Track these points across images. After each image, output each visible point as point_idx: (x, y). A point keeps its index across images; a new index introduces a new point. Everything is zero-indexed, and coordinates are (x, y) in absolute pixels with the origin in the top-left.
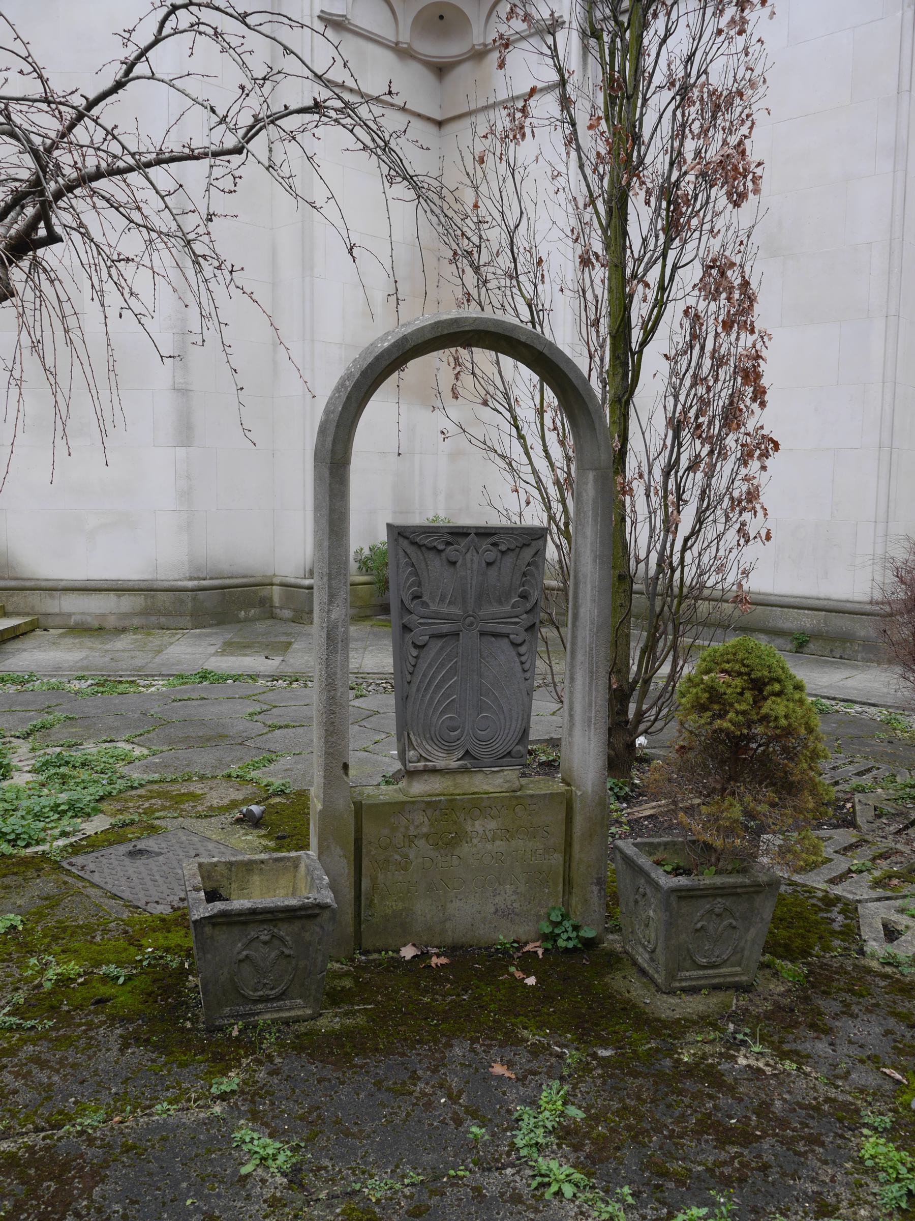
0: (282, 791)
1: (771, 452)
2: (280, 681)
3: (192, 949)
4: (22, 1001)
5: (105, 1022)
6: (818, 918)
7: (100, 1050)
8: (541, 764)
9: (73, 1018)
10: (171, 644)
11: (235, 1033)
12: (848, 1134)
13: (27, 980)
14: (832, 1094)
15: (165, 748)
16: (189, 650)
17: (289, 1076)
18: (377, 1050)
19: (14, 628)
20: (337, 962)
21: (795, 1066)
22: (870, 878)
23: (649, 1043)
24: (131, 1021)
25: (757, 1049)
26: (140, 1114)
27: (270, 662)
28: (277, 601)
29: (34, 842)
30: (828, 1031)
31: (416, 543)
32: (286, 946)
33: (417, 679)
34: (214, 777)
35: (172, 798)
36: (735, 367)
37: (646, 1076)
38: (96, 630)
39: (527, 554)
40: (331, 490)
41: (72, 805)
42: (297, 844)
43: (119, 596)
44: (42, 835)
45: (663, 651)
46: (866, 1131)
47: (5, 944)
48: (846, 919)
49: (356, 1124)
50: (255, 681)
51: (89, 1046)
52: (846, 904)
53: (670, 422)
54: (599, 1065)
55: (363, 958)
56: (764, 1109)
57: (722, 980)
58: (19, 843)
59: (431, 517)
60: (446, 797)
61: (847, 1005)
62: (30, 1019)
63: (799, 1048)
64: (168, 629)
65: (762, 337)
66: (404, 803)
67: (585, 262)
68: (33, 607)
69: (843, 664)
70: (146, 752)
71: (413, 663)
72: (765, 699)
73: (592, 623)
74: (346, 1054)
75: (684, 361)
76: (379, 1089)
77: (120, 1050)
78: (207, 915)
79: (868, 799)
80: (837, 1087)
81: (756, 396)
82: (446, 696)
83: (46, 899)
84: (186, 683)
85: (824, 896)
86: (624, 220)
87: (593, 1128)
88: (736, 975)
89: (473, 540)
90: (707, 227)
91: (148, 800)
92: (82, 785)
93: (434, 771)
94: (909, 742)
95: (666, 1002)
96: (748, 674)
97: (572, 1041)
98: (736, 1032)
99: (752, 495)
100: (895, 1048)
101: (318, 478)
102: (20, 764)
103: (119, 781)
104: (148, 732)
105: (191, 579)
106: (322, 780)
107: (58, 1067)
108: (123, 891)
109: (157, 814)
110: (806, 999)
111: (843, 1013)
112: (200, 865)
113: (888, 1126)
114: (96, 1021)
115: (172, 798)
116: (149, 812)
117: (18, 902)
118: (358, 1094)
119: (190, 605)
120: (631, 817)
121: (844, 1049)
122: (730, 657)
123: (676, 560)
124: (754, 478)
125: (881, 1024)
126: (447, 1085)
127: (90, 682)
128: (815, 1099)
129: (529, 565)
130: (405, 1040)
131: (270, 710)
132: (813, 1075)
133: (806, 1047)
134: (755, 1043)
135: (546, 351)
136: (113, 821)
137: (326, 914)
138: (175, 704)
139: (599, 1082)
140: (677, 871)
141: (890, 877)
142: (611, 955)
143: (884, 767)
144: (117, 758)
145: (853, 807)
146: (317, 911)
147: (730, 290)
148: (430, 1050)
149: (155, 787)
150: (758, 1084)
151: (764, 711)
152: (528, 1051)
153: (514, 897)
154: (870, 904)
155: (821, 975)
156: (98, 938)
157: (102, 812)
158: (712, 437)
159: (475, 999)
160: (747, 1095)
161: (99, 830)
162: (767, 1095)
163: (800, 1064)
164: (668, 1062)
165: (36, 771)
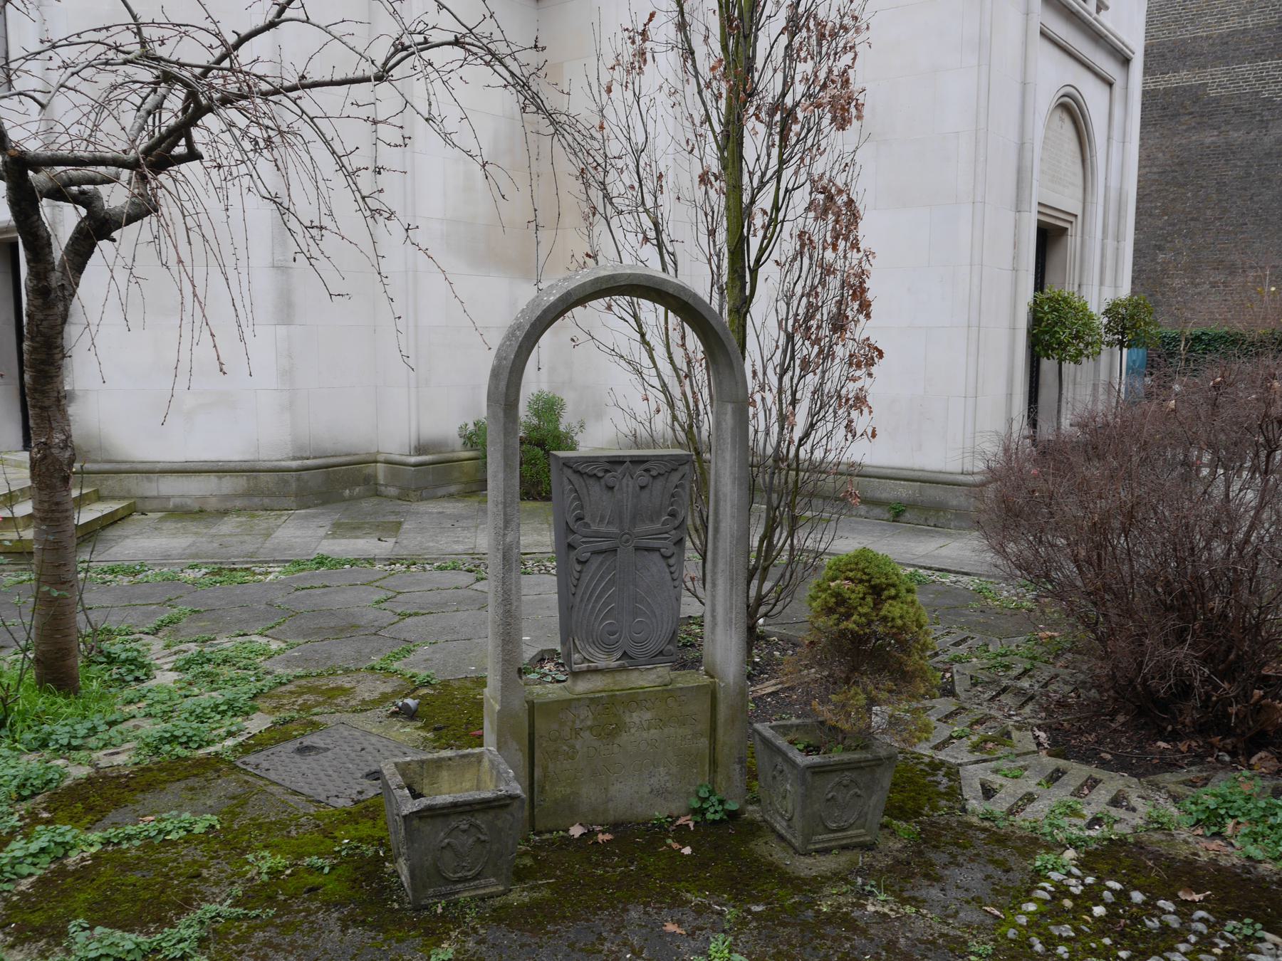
0: (428, 682)
1: (876, 359)
2: (398, 565)
4: (240, 893)
5: (319, 909)
6: (926, 781)
11: (440, 911)
14: (945, 930)
15: (301, 641)
16: (298, 533)
18: (565, 917)
19: (112, 514)
21: (914, 910)
22: (969, 743)
24: (344, 905)
25: (882, 898)
27: (383, 544)
28: (381, 479)
30: (939, 879)
31: (579, 472)
32: (481, 833)
34: (358, 670)
35: (323, 693)
37: (794, 925)
38: (196, 513)
40: (505, 429)
41: (230, 704)
44: (211, 737)
50: (373, 565)
51: (313, 930)
52: (949, 768)
54: (753, 919)
57: (849, 841)
58: (191, 745)
59: (536, 393)
61: (954, 856)
63: (917, 894)
64: (272, 510)
65: (867, 256)
68: (129, 491)
69: (937, 532)
70: (283, 646)
73: (732, 536)
74: (539, 923)
76: (573, 950)
78: (415, 810)
79: (965, 668)
80: (948, 924)
82: (606, 604)
83: (234, 798)
84: (303, 569)
85: (931, 762)
92: (231, 683)
93: (596, 671)
94: (999, 611)
96: (869, 581)
97: (729, 900)
98: (864, 884)
100: (994, 890)
104: (279, 624)
105: (294, 459)
110: (920, 853)
111: (951, 863)
112: (396, 764)
113: (990, 952)
115: (323, 693)
116: (305, 708)
117: (208, 803)
119: (294, 485)
120: (755, 695)
121: (953, 893)
122: (853, 566)
127: (204, 571)
128: (932, 935)
129: (676, 487)
133: (921, 894)
135: (690, 301)
136: (273, 719)
137: (516, 804)
139: (755, 932)
140: (808, 750)
141: (986, 741)
143: (978, 636)
145: (952, 676)
146: (508, 802)
148: (610, 915)
149: (303, 682)
150: (885, 926)
151: (883, 613)
153: (667, 778)
156: (293, 833)
157: (258, 709)
160: (877, 935)
163: (918, 907)
164: (810, 913)
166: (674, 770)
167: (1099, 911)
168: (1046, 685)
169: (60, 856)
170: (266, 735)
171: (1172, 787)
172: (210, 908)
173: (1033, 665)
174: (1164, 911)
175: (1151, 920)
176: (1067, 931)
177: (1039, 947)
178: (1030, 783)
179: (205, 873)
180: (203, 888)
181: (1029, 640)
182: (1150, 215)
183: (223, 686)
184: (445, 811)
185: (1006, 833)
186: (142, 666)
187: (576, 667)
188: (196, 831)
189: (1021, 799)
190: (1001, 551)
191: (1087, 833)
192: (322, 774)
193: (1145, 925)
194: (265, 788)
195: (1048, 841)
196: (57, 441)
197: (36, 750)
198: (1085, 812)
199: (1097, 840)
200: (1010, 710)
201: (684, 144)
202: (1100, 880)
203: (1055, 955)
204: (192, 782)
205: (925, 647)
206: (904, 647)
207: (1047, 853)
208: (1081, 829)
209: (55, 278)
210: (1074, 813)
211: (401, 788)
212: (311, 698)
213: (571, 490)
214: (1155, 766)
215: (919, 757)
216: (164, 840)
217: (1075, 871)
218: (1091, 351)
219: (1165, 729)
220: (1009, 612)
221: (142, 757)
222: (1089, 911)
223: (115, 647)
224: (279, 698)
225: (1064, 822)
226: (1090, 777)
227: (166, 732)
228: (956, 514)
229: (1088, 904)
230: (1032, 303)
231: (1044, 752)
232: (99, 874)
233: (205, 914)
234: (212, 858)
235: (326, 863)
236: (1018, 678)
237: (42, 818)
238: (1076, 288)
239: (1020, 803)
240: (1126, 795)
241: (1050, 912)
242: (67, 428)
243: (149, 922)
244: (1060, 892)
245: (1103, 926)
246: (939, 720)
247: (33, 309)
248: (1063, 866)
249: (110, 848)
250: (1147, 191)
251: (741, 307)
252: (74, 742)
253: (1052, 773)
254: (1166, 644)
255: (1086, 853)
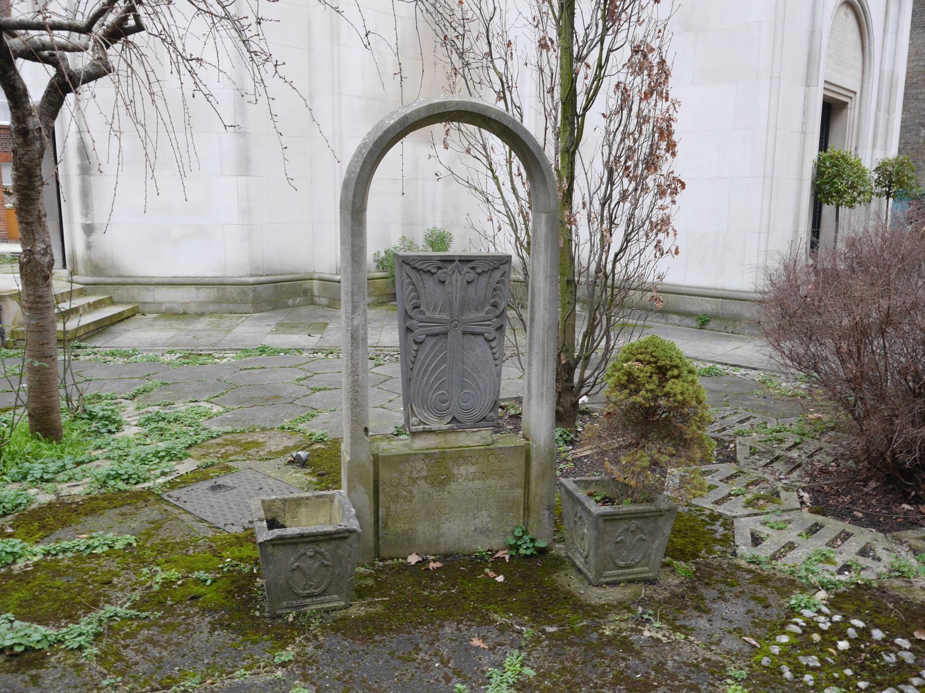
0: (321, 439)
1: (679, 189)
3: (258, 559)
4: (138, 598)
5: (197, 613)
6: (705, 529)
7: (195, 633)
8: (511, 417)
9: (175, 610)
10: (238, 325)
11: (291, 619)
12: (717, 683)
13: (142, 584)
14: (708, 655)
16: (251, 330)
17: (329, 649)
19: (120, 314)
20: (362, 566)
23: (582, 622)
24: (216, 611)
26: (225, 677)
28: (316, 292)
29: (142, 480)
30: (707, 611)
32: (325, 559)
33: (417, 367)
34: (272, 429)
36: (654, 126)
37: (579, 645)
38: (181, 314)
39: (497, 275)
40: (353, 230)
41: (168, 452)
42: (333, 480)
43: (198, 289)
44: (148, 475)
45: (599, 335)
46: (729, 681)
47: (124, 557)
48: (725, 530)
49: (376, 682)
50: (301, 353)
51: (187, 630)
52: (725, 519)
53: (606, 164)
55: (381, 563)
56: (660, 667)
57: (635, 576)
59: (431, 228)
60: (439, 450)
62: (145, 611)
63: (687, 623)
64: (235, 313)
66: (409, 455)
67: (543, 45)
68: (133, 298)
69: (734, 337)
70: (221, 409)
71: (414, 355)
72: (667, 380)
73: (544, 324)
74: (369, 633)
75: (617, 119)
76: (392, 658)
77: (210, 632)
78: (268, 539)
79: (746, 441)
80: (712, 651)
81: (669, 148)
82: (438, 378)
83: (152, 523)
85: (711, 514)
86: (572, 15)
87: (541, 683)
88: (644, 573)
89: (457, 265)
90: (634, 19)
91: (223, 447)
92: (175, 436)
93: (430, 432)
94: (778, 397)
95: (595, 592)
96: (656, 363)
97: (528, 621)
98: (643, 613)
99: (665, 221)
100: (753, 622)
101: (343, 221)
102: (129, 420)
103: (203, 432)
104: (223, 394)
105: (252, 276)
106: (350, 440)
107: (166, 645)
108: (208, 516)
109: (231, 458)
110: (694, 589)
111: (719, 598)
112: (263, 501)
113: (745, 677)
114: (192, 612)
115: (241, 445)
116: (225, 456)
117: (133, 526)
118: (378, 661)
119: (251, 295)
120: (575, 456)
121: (718, 623)
123: (609, 267)
124: (668, 207)
125: (745, 606)
126: (440, 654)
127: (178, 355)
128: (696, 659)
129: (498, 282)
130: (411, 622)
131: (312, 376)
132: (696, 642)
133: (691, 623)
134: (656, 621)
135: (510, 126)
136: (199, 463)
137: (354, 537)
138: (242, 372)
139: (546, 650)
140: (605, 501)
141: (758, 499)
142: (557, 559)
143: (758, 416)
144: (200, 415)
145: (735, 447)
146: (347, 535)
147: (651, 68)
149: (229, 437)
150: (657, 649)
151: (666, 389)
152: (497, 629)
153: (488, 520)
154: (742, 519)
155: (705, 571)
156: (191, 552)
157: (190, 456)
158: (636, 177)
159: (460, 592)
160: (649, 657)
161: (189, 471)
162: (663, 657)
163: (687, 635)
164: (595, 635)
165: (139, 425)
166: (494, 513)
167: (843, 645)
168: (811, 456)
169: (10, 562)
170: (191, 476)
171: (913, 542)
172: (110, 609)
173: (802, 440)
174: (900, 648)
175: (888, 656)
176: (813, 661)
177: (788, 675)
178: (792, 534)
179: (115, 580)
180: (110, 593)
181: (801, 420)
182: (917, 99)
183: (169, 438)
184: (294, 540)
185: (768, 575)
186: (115, 422)
187: (413, 428)
188: (116, 547)
189: (783, 547)
190: (778, 348)
191: (838, 577)
192: (225, 507)
193: (883, 660)
194: (178, 516)
195: (803, 583)
196: (39, 249)
197: (19, 481)
198: (837, 560)
199: (846, 584)
200: (780, 474)
201: (531, 21)
202: (846, 618)
203: (801, 682)
204: (124, 510)
205: (702, 419)
206: (685, 419)
207: (801, 593)
208: (832, 574)
209: (34, 122)
210: (828, 560)
211: (261, 520)
212: (231, 449)
213: (409, 283)
214: (900, 524)
215: (701, 510)
216: (91, 553)
217: (825, 610)
218: (862, 198)
219: (909, 494)
220: (786, 399)
221: (92, 489)
222: (834, 645)
223: (97, 409)
224: (208, 448)
225: (818, 568)
226: (843, 531)
227: (113, 470)
228: (749, 324)
229: (834, 639)
230: (816, 159)
231: (807, 509)
232: (34, 578)
233: (105, 613)
234: (123, 569)
235: (210, 577)
236: (789, 449)
237: (6, 533)
238: (853, 148)
239: (782, 550)
240: (873, 547)
241: (801, 644)
242: (47, 239)
243: (61, 618)
244: (811, 627)
245: (846, 659)
246: (721, 481)
247: (16, 146)
248: (815, 605)
249: (49, 558)
250: (915, 80)
251: (570, 150)
252: (46, 476)
253: (812, 526)
254: (913, 423)
255: (836, 594)
